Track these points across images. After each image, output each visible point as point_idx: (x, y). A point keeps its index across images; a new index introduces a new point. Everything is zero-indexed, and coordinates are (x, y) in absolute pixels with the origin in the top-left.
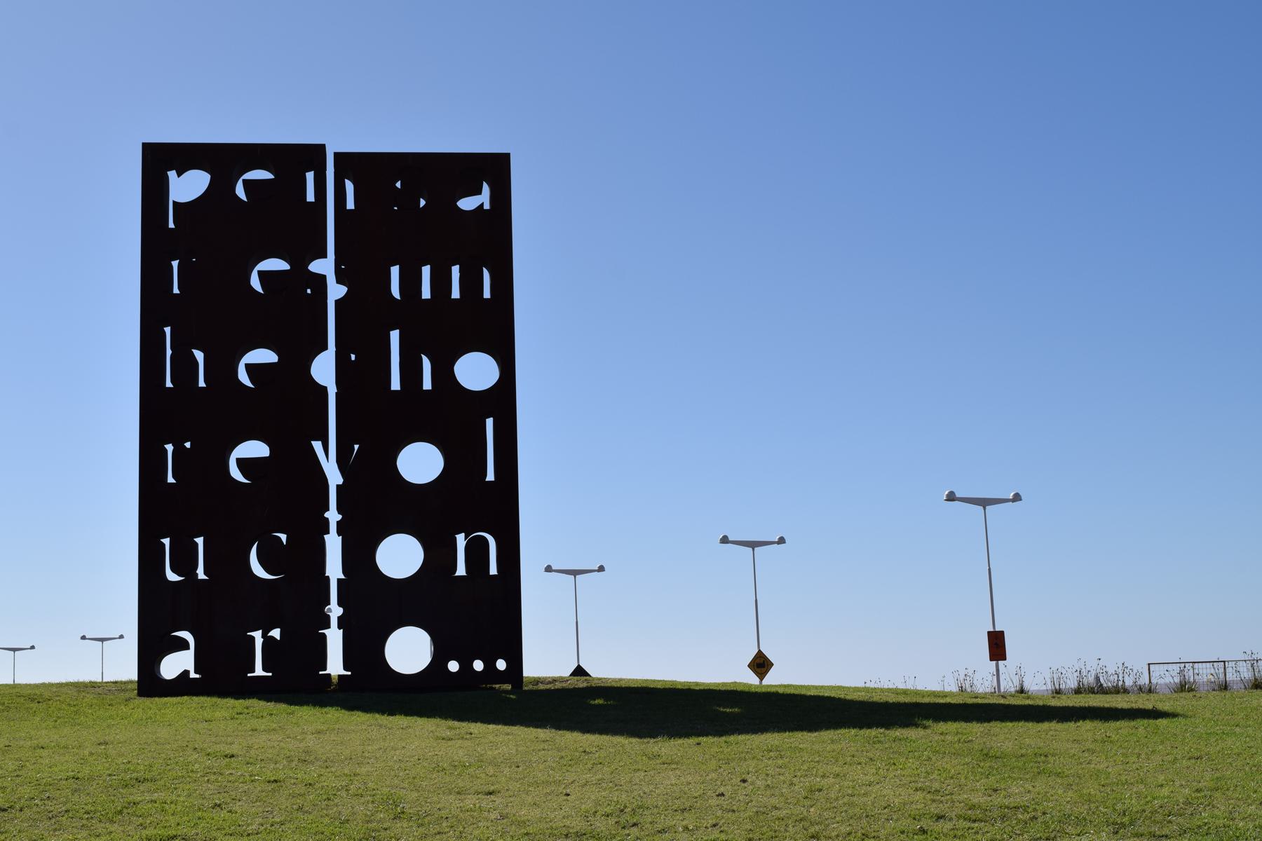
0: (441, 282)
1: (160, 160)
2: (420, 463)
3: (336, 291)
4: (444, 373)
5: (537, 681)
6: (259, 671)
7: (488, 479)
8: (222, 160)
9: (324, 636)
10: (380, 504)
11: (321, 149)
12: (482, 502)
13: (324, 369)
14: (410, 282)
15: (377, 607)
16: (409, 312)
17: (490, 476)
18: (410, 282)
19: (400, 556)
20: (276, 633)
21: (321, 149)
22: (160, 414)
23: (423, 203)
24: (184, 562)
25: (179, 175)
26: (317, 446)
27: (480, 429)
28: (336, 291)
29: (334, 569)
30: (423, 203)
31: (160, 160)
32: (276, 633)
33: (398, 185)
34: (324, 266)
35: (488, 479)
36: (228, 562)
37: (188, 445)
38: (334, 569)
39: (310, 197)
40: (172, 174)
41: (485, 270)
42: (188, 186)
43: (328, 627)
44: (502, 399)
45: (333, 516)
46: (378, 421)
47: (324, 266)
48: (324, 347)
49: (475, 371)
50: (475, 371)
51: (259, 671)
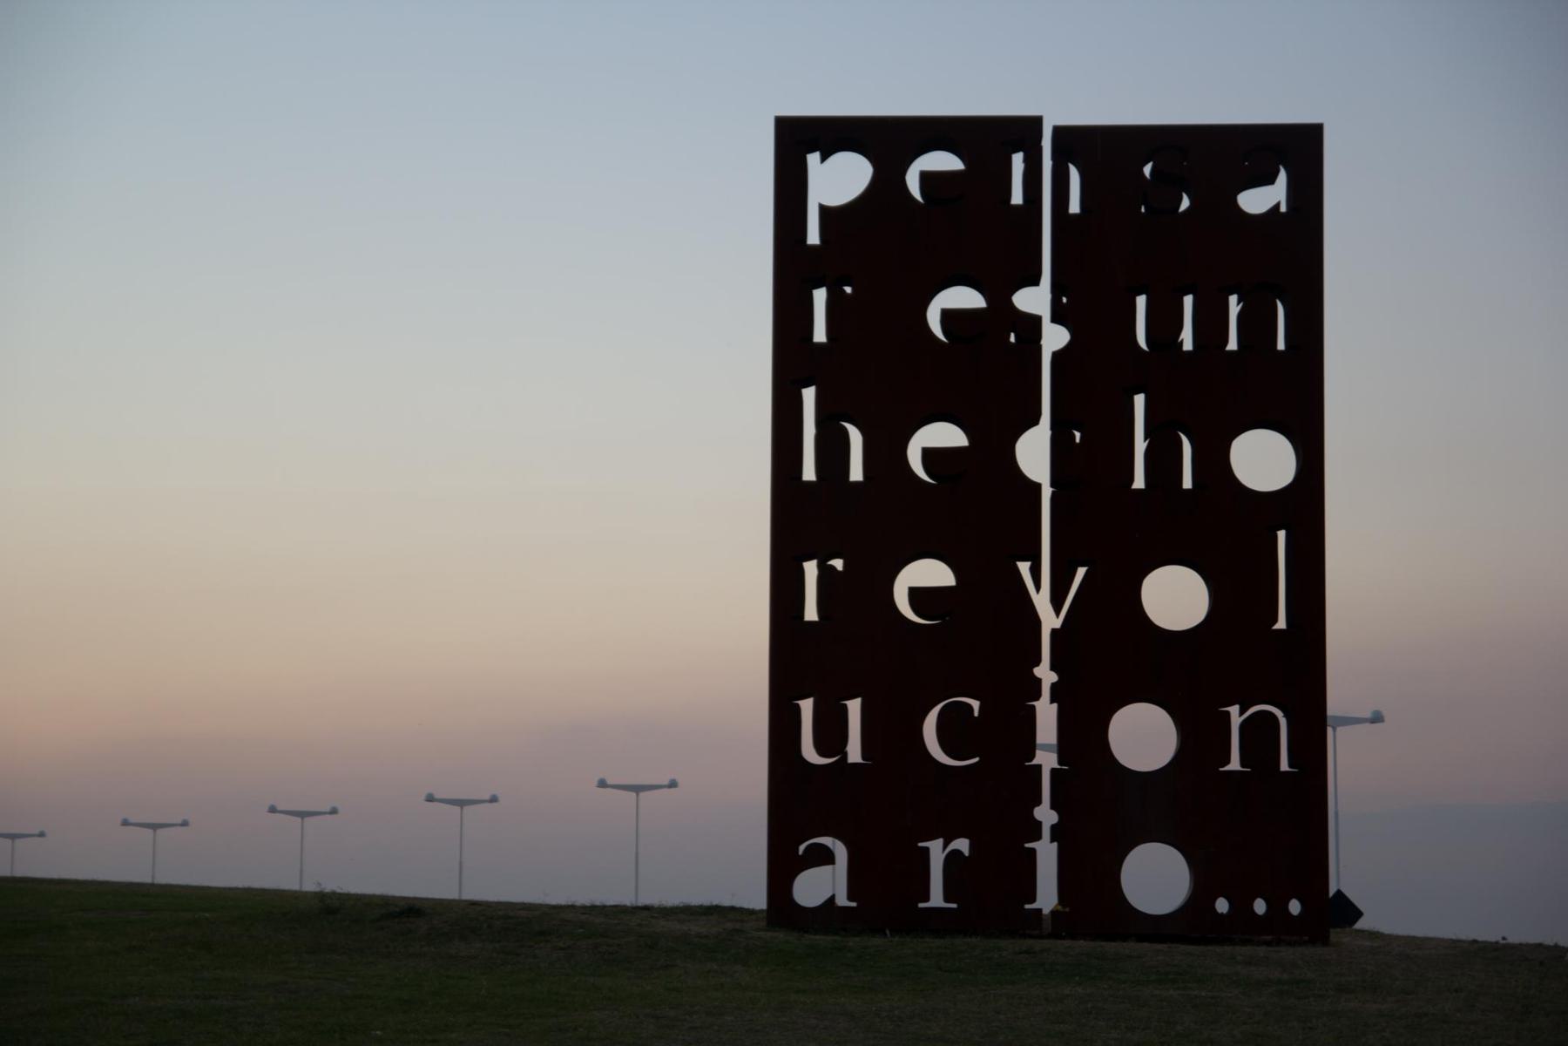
1: (799, 140)
3: (1055, 338)
8: (888, 140)
10: (1115, 654)
11: (1035, 123)
13: (1034, 453)
26: (1024, 567)
31: (799, 140)
39: (1017, 198)
40: (813, 159)
42: (839, 179)
47: (1034, 300)
49: (1262, 460)
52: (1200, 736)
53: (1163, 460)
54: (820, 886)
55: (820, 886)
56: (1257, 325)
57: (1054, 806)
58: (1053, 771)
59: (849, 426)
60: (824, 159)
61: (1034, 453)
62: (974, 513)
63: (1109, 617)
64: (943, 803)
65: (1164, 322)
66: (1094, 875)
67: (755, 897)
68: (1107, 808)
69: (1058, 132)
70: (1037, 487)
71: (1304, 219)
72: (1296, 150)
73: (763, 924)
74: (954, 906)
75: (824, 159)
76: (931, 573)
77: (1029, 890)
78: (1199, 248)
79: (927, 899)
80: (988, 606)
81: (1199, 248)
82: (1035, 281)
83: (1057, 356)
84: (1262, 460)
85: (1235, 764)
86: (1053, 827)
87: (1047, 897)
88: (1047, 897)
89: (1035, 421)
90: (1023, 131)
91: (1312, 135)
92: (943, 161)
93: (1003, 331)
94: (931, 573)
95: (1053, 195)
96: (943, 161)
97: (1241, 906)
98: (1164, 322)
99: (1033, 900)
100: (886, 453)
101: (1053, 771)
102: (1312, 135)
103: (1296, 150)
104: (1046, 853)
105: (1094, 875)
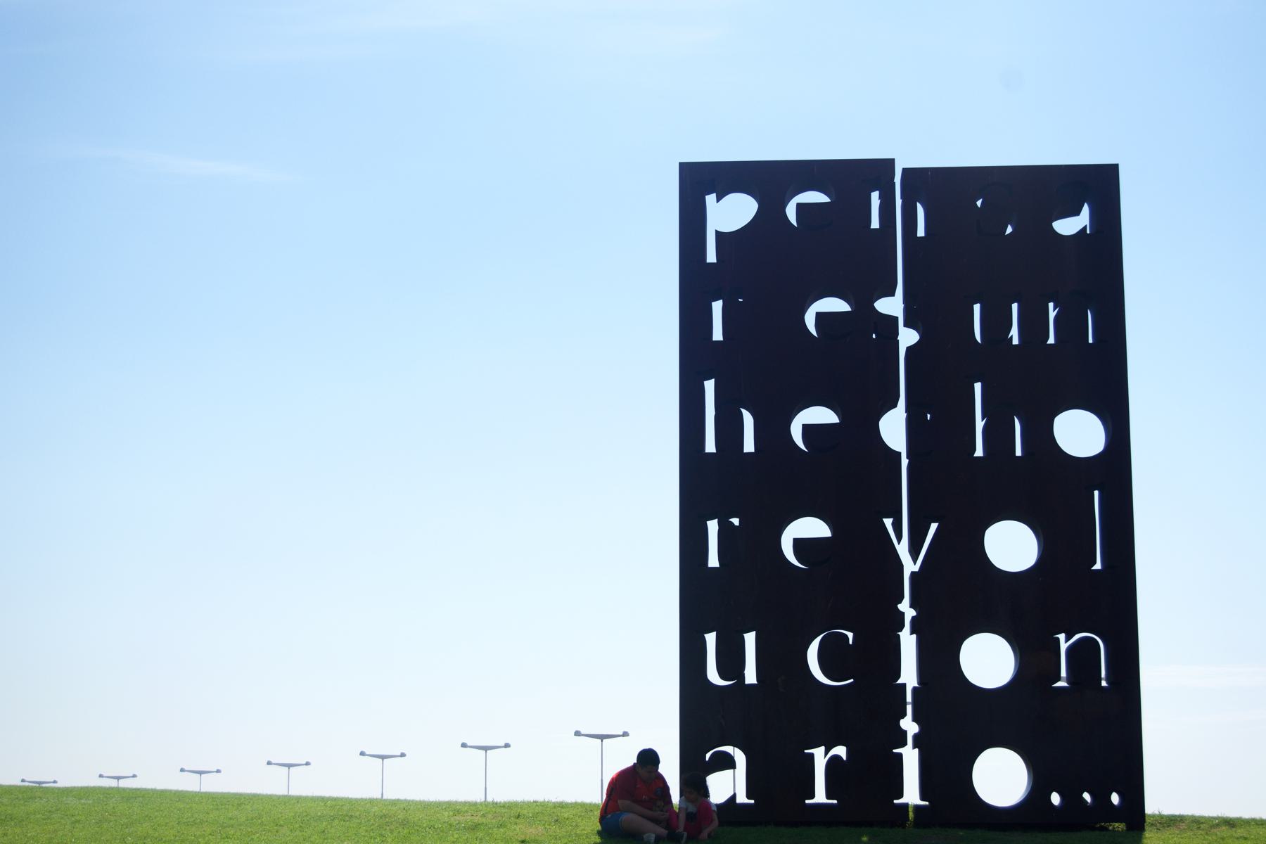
0: (1034, 325)
1: (700, 182)
2: (1011, 546)
3: (908, 337)
4: (1041, 436)
5: (1153, 816)
6: (820, 796)
7: (976, 455)
8: (770, 181)
9: (900, 755)
10: (962, 594)
11: (890, 163)
12: (1089, 594)
13: (893, 429)
14: (996, 323)
15: (962, 723)
16: (992, 357)
17: (979, 452)
18: (996, 323)
19: (988, 661)
20: (841, 751)
21: (890, 163)
22: (708, 484)
23: (1009, 230)
24: (731, 661)
25: (718, 200)
26: (888, 522)
27: (1091, 511)
28: (908, 337)
29: (909, 676)
30: (1009, 230)
31: (700, 182)
32: (841, 751)
33: (979, 203)
34: (891, 306)
35: (976, 455)
36: (781, 660)
37: (736, 521)
38: (909, 676)
39: (875, 224)
40: (711, 199)
41: (919, 206)
42: (731, 213)
43: (904, 744)
44: (1114, 466)
45: (906, 608)
46: (960, 496)
47: (891, 306)
48: (894, 405)
49: (1078, 433)
50: (1078, 433)
51: (820, 796)
53: (998, 435)
61: (893, 429)
68: (962, 723)
71: (1105, 242)
72: (1097, 186)
79: (813, 796)
87: (911, 794)
88: (911, 794)
94: (812, 527)
99: (901, 796)
103: (1097, 186)
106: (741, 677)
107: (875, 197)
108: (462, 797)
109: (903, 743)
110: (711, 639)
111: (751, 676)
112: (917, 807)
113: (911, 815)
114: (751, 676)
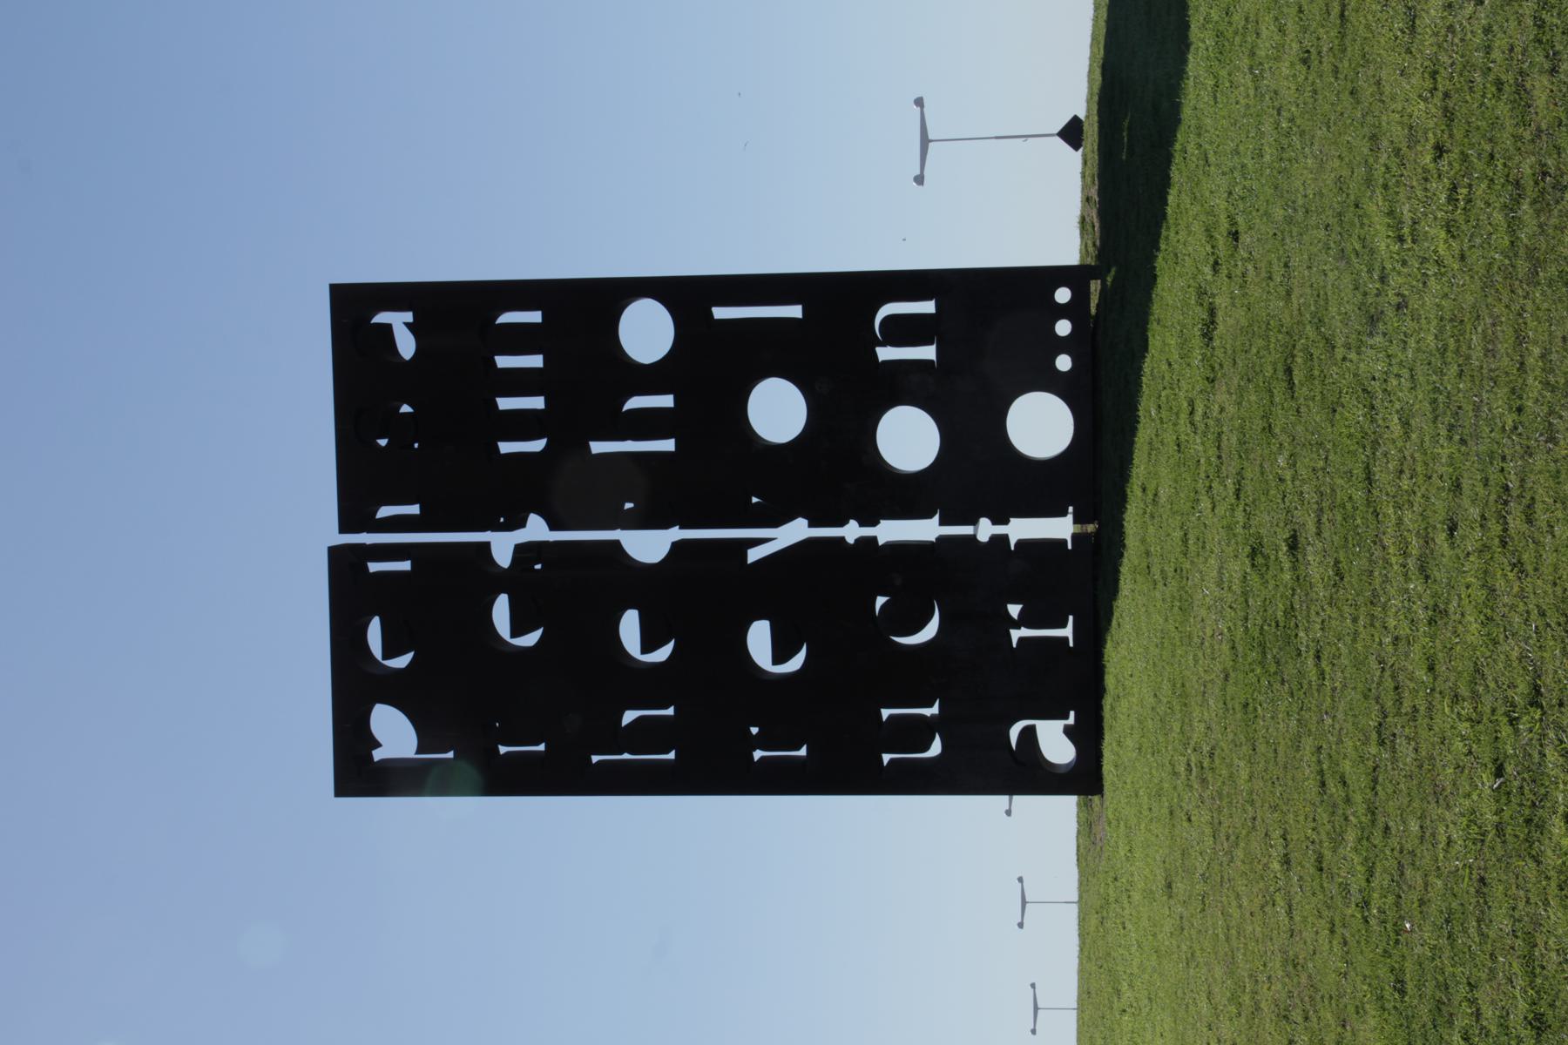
1: (359, 771)
3: (536, 529)
5: (1085, 251)
8: (355, 688)
10: (834, 468)
11: (335, 553)
12: (831, 328)
13: (648, 546)
15: (980, 470)
20: (1014, 610)
21: (335, 553)
23: (406, 409)
24: (903, 330)
26: (754, 555)
29: (926, 530)
30: (406, 409)
31: (359, 771)
34: (503, 547)
38: (926, 530)
39: (406, 566)
40: (378, 755)
42: (394, 734)
47: (503, 547)
49: (646, 333)
52: (903, 386)
53: (648, 424)
54: (1055, 742)
55: (1055, 742)
56: (520, 340)
57: (841, 523)
58: (942, 523)
59: (672, 644)
60: (378, 745)
61: (648, 546)
62: (700, 598)
63: (792, 479)
64: (975, 624)
65: (522, 425)
66: (1037, 486)
67: (1065, 806)
68: (980, 470)
69: (344, 528)
70: (677, 547)
71: (430, 302)
72: (353, 308)
73: (1096, 799)
74: (1071, 618)
75: (378, 745)
76: (759, 639)
77: (1052, 547)
78: (443, 392)
79: (1066, 639)
80: (792, 591)
81: (443, 392)
82: (486, 546)
83: (553, 526)
84: (646, 333)
85: (503, 750)
86: (995, 523)
87: (1061, 528)
88: (1061, 528)
89: (617, 544)
90: (345, 564)
91: (341, 295)
92: (374, 634)
93: (533, 578)
94: (759, 639)
95: (402, 535)
96: (374, 634)
97: (1063, 345)
98: (522, 425)
99: (1065, 541)
100: (647, 686)
101: (942, 523)
102: (341, 295)
103: (353, 308)
104: (1021, 529)
105: (1037, 486)
106: (883, 344)
107: (374, 567)
108: (1074, 1026)
109: (1004, 539)
110: (928, 307)
111: (885, 353)
112: (1076, 522)
113: (1091, 528)
114: (885, 353)
